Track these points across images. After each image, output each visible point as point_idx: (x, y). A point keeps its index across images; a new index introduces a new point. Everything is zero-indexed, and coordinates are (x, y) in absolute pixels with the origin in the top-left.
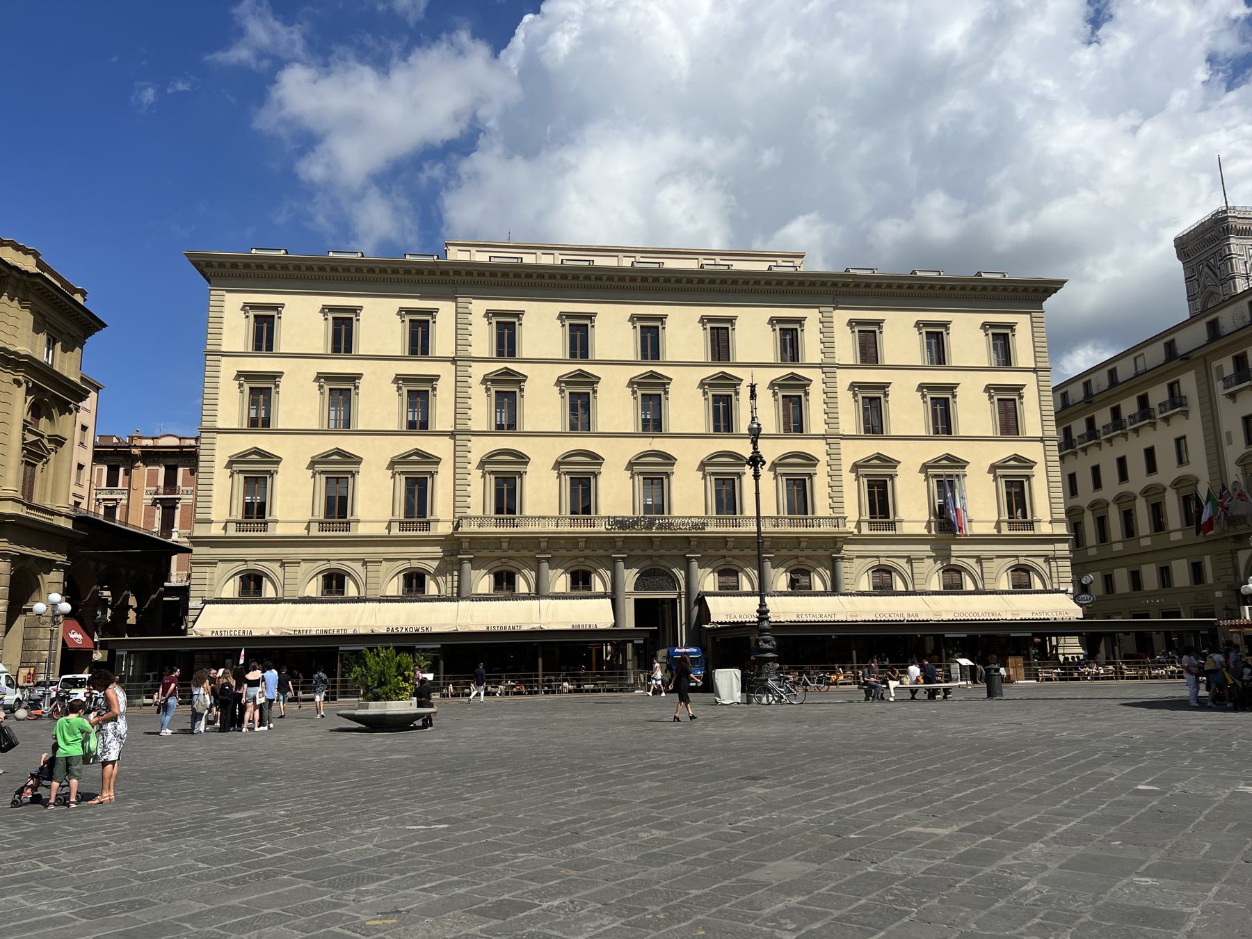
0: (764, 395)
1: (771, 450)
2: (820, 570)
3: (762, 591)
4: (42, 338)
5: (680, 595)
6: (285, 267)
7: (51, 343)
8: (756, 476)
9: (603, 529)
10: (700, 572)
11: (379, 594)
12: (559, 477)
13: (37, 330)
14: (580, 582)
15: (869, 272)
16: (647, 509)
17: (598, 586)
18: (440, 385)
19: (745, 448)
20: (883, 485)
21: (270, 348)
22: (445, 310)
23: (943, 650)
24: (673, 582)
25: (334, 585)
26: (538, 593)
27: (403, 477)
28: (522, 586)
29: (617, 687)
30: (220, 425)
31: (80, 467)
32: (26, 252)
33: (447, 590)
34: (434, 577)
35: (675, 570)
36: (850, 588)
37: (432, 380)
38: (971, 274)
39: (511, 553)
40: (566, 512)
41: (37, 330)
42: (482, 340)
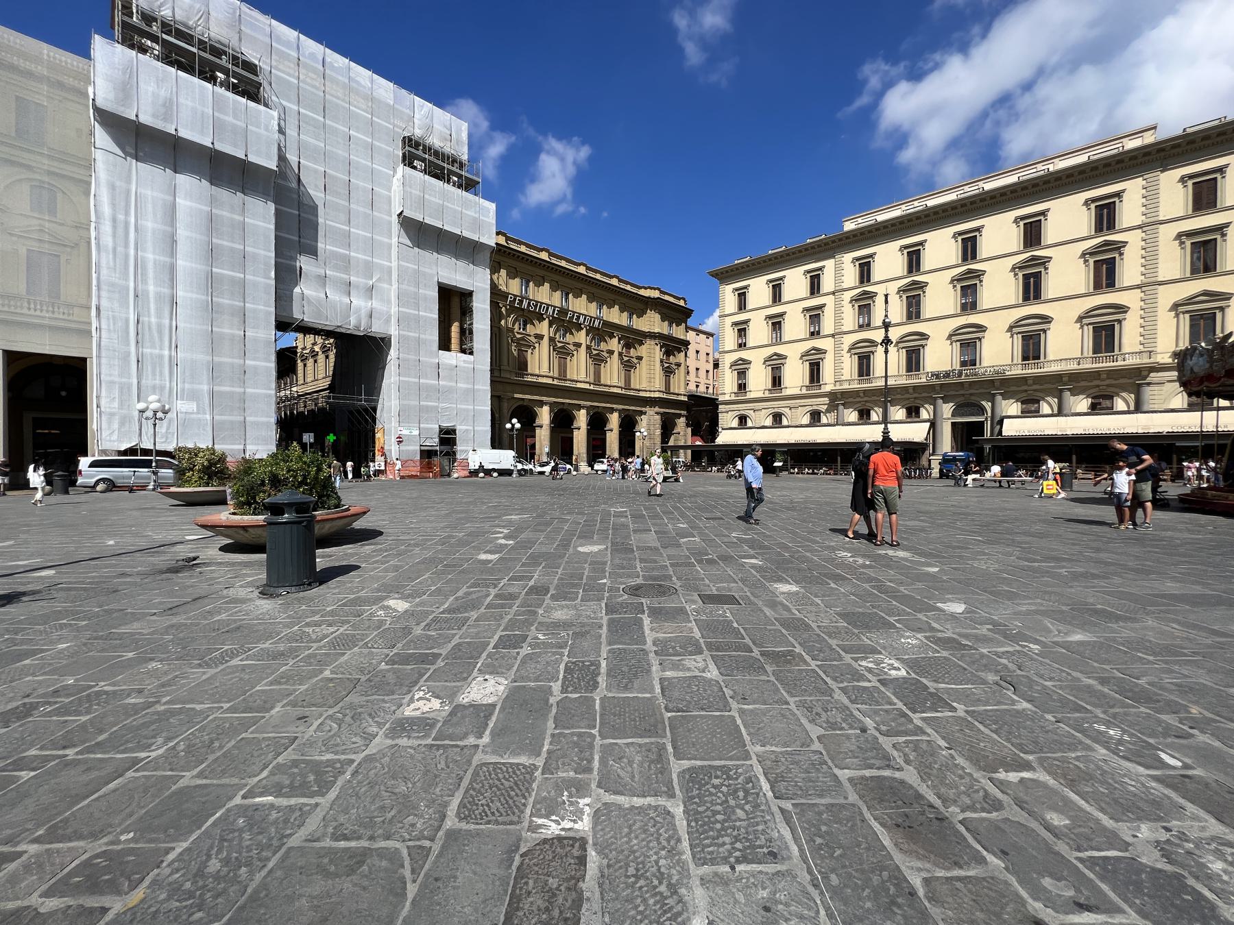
0: (894, 300)
1: (894, 334)
2: (1124, 394)
3: (885, 420)
4: (666, 323)
5: (986, 419)
6: (788, 255)
7: (670, 325)
8: (886, 352)
9: (924, 380)
10: (1004, 402)
11: (798, 424)
12: (1012, 336)
13: (663, 320)
14: (864, 416)
15: (1217, 122)
16: (963, 364)
17: (924, 414)
18: (826, 309)
19: (878, 336)
20: (818, 364)
21: (780, 301)
22: (829, 264)
23: (1175, 456)
24: (982, 410)
25: (777, 418)
26: (839, 423)
27: (1020, 336)
28: (1045, 409)
29: (832, 472)
30: (1160, 279)
31: (707, 371)
32: (655, 289)
33: (832, 421)
34: (825, 414)
35: (983, 403)
36: (1152, 407)
37: (821, 307)
38: (1179, 132)
39: (866, 399)
40: (856, 376)
41: (663, 320)
42: (850, 275)
